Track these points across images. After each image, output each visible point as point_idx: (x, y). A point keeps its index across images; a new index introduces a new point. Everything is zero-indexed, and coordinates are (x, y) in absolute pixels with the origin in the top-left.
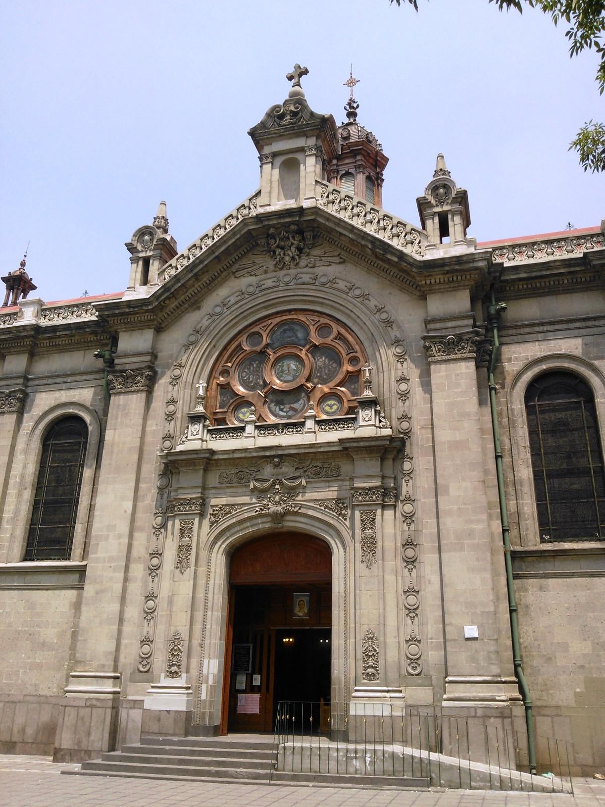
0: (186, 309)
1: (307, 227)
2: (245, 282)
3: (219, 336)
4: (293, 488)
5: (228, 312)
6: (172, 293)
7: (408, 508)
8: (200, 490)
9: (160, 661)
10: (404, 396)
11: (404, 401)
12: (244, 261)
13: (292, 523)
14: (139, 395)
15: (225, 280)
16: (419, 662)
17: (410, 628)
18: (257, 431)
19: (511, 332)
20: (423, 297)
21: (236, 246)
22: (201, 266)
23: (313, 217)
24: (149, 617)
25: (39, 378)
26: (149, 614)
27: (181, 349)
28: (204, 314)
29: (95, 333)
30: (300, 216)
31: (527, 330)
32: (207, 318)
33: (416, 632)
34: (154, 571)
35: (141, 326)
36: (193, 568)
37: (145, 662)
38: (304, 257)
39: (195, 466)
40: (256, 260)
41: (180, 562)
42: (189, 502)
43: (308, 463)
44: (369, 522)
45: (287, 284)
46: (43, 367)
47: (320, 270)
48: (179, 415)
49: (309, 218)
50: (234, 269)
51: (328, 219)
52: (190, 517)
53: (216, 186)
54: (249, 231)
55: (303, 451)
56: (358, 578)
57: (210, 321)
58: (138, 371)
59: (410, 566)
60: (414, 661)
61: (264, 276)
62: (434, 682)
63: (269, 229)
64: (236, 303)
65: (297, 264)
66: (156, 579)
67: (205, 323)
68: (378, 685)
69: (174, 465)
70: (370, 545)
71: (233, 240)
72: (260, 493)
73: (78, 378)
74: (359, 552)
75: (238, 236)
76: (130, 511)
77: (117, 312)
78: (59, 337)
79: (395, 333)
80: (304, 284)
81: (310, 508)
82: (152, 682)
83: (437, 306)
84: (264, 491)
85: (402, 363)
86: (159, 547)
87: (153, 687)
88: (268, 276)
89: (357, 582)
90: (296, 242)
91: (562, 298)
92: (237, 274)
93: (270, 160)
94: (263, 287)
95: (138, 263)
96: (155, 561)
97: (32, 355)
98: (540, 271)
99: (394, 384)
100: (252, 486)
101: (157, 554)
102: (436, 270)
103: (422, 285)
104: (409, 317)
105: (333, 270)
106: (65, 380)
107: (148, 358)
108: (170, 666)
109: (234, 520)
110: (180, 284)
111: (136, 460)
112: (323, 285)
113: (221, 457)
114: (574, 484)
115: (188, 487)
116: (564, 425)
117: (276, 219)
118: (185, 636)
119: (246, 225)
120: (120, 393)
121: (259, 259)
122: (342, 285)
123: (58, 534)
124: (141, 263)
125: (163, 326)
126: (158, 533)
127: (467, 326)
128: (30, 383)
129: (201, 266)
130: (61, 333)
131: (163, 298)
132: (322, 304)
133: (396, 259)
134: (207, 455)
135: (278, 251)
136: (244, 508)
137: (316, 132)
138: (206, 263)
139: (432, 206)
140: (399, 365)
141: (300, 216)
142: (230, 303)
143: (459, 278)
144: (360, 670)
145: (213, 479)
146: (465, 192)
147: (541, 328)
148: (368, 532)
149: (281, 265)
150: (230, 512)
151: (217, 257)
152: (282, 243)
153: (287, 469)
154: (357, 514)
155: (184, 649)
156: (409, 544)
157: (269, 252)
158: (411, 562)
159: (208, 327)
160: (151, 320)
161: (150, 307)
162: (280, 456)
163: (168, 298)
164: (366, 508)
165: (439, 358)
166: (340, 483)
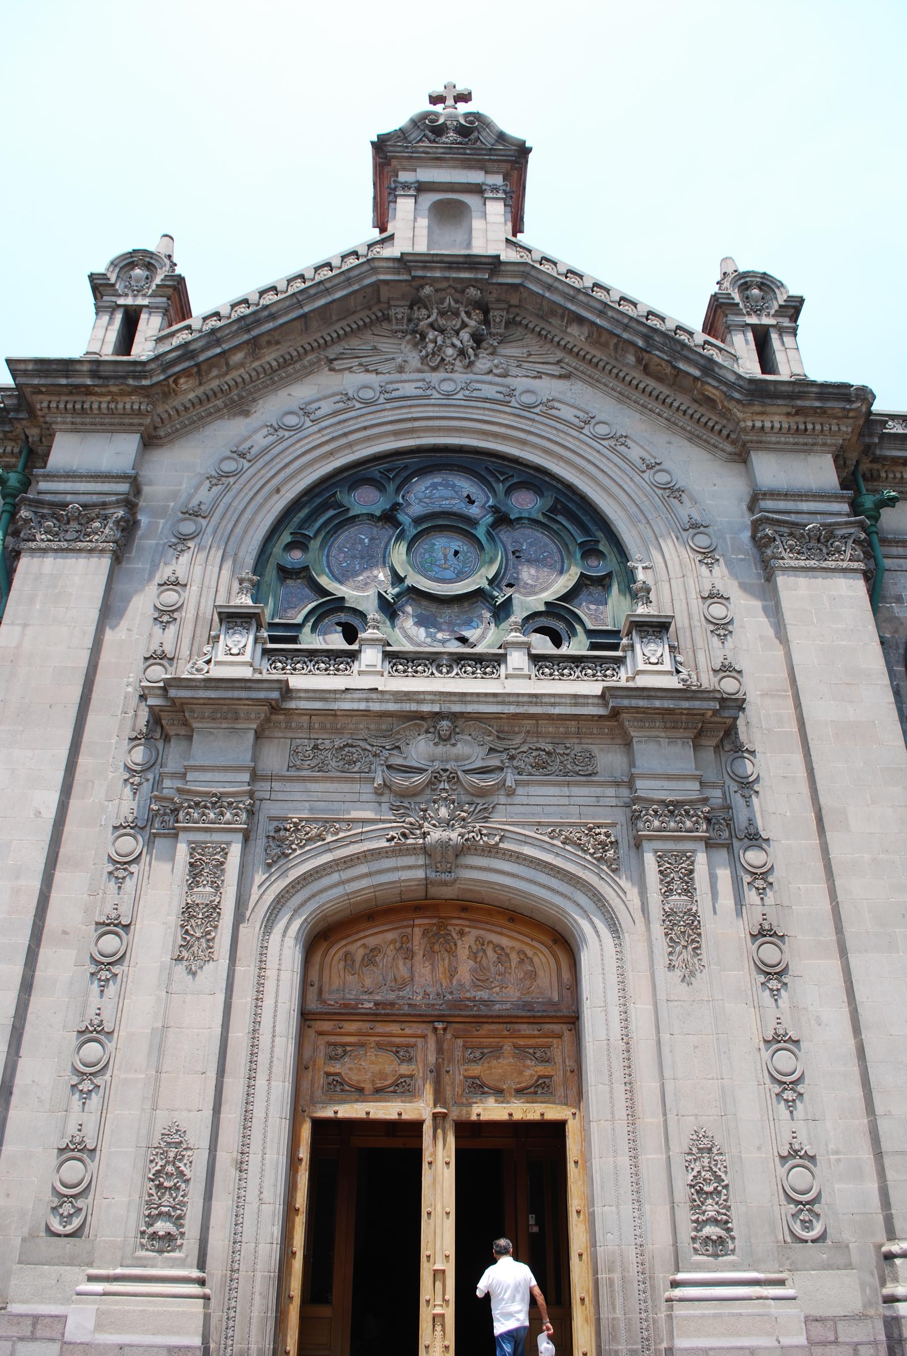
0: (219, 410)
1: (498, 301)
2: (353, 381)
3: (288, 471)
4: (483, 793)
5: (315, 428)
6: (198, 365)
7: (753, 857)
8: (246, 777)
9: (117, 1203)
10: (722, 628)
11: (723, 638)
12: (354, 342)
15: (308, 371)
16: (816, 1208)
17: (788, 1128)
18: (387, 666)
19: (894, 551)
20: (741, 457)
21: (342, 309)
22: (271, 325)
23: (517, 281)
24: (86, 1086)
26: (87, 1079)
27: (201, 483)
32: (265, 431)
33: (802, 1137)
34: (106, 968)
35: (112, 424)
36: (224, 962)
37: (67, 1209)
38: (483, 354)
41: (186, 946)
42: (218, 801)
43: (518, 740)
45: (448, 395)
47: (520, 383)
48: (189, 614)
50: (331, 353)
51: (550, 287)
52: (217, 837)
53: (277, 219)
54: (377, 285)
56: (662, 1005)
57: (271, 438)
59: (774, 984)
60: (806, 1206)
61: (397, 376)
62: (855, 1258)
63: (422, 287)
65: (471, 364)
66: (112, 989)
67: (260, 440)
68: (734, 1267)
70: (684, 930)
74: (661, 944)
75: (356, 287)
76: (50, 813)
77: (63, 381)
79: (685, 511)
80: (486, 400)
82: (90, 1264)
83: (771, 470)
84: (406, 794)
85: (709, 566)
86: (123, 910)
87: (91, 1279)
88: (404, 376)
89: (663, 1013)
90: (472, 323)
92: (337, 365)
94: (395, 394)
96: (110, 943)
99: (696, 604)
100: (379, 781)
101: (116, 926)
102: (780, 402)
103: (744, 430)
104: (717, 489)
105: (548, 388)
107: (124, 487)
108: (151, 1220)
110: (218, 350)
111: (77, 699)
112: (528, 407)
113: (303, 705)
115: (217, 761)
117: (441, 269)
118: (198, 1138)
119: (375, 270)
120: (45, 551)
121: (386, 345)
122: (567, 413)
124: (119, 317)
125: (162, 433)
126: (121, 874)
127: (839, 514)
129: (271, 325)
131: (177, 369)
132: (524, 443)
134: (275, 695)
135: (431, 335)
136: (359, 834)
138: (281, 321)
139: (739, 313)
140: (704, 570)
142: (319, 413)
143: (818, 427)
144: (686, 1231)
145: (275, 758)
146: (801, 300)
148: (678, 900)
151: (304, 316)
152: (442, 322)
153: (469, 751)
154: (650, 859)
155: (196, 1171)
156: (765, 934)
157: (414, 332)
158: (774, 975)
159: (265, 450)
160: (139, 413)
161: (145, 382)
162: (454, 717)
163: (186, 372)
164: (670, 845)
165: (793, 563)
166: (598, 791)
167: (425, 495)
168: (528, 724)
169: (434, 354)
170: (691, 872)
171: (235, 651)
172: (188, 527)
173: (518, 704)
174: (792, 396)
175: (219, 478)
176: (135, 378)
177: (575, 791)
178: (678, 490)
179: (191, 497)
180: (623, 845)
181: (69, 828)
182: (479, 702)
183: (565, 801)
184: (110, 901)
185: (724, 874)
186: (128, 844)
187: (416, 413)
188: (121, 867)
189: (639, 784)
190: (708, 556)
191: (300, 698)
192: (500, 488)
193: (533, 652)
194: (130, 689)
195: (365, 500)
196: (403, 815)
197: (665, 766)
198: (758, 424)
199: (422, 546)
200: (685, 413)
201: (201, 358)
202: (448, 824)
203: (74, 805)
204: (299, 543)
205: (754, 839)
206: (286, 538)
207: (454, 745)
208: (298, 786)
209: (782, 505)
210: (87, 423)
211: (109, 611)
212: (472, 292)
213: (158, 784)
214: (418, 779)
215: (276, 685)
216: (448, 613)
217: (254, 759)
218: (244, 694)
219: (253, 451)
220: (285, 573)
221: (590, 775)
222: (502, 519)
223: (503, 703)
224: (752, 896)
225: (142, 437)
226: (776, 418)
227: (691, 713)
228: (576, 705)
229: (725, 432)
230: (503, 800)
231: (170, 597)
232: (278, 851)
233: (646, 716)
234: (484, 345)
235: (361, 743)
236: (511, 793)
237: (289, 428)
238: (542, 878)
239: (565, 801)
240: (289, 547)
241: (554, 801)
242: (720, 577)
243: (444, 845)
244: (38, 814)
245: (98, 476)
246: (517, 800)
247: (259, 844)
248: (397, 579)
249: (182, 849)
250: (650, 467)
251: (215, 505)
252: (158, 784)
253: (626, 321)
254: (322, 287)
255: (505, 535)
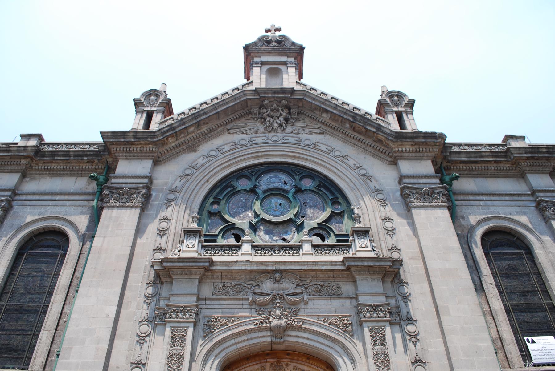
0: (184, 150)
1: (294, 105)
2: (237, 137)
3: (212, 173)
4: (294, 304)
5: (223, 156)
6: (176, 132)
7: (410, 328)
8: (195, 299)
10: (391, 232)
11: (391, 236)
12: (238, 122)
13: (295, 338)
14: (133, 210)
15: (219, 134)
18: (253, 251)
19: (459, 198)
21: (233, 110)
22: (205, 117)
23: (301, 97)
25: (27, 194)
27: (177, 179)
28: (200, 155)
29: (90, 162)
30: (291, 95)
31: (471, 198)
32: (202, 158)
35: (141, 156)
38: (289, 125)
39: (191, 274)
40: (248, 124)
42: (183, 310)
43: (308, 281)
44: (379, 339)
45: (275, 142)
46: (31, 186)
47: (304, 136)
48: (171, 231)
49: (299, 97)
50: (229, 127)
51: (314, 99)
52: (182, 325)
55: (306, 268)
57: (205, 161)
58: (132, 191)
61: (255, 135)
63: (264, 100)
64: (230, 150)
65: (284, 129)
67: (201, 161)
69: (165, 273)
71: (234, 103)
72: (261, 307)
73: (67, 198)
75: (238, 101)
78: (56, 162)
79: (373, 184)
80: (290, 143)
81: (313, 324)
83: (407, 167)
84: (262, 305)
86: (142, 357)
90: (284, 114)
91: (488, 179)
92: (231, 131)
93: (259, 65)
94: (254, 142)
95: (142, 113)
97: (24, 176)
98: (476, 157)
99: (379, 222)
100: (251, 299)
102: (408, 140)
104: (385, 176)
105: (315, 138)
106: (54, 198)
107: (146, 181)
109: (229, 333)
110: (184, 127)
112: (308, 146)
114: (534, 317)
115: (183, 292)
116: (514, 270)
117: (272, 94)
121: (250, 123)
122: (323, 147)
123: (17, 341)
124: (145, 115)
126: (142, 341)
128: (17, 198)
129: (205, 117)
130: (59, 158)
131: (168, 134)
132: (306, 160)
133: (374, 130)
135: (268, 119)
137: (295, 55)
139: (390, 107)
140: (382, 208)
141: (291, 95)
142: (224, 150)
145: (207, 291)
146: (414, 101)
147: (481, 198)
148: (379, 348)
149: (270, 129)
150: (226, 324)
151: (218, 113)
152: (272, 114)
153: (288, 286)
154: (366, 330)
159: (203, 165)
161: (155, 140)
162: (281, 272)
163: (171, 136)
164: (374, 324)
165: (418, 204)
167: (267, 181)
168: (313, 274)
169: (269, 126)
170: (384, 335)
171: (190, 246)
172: (171, 196)
173: (308, 265)
174: (413, 138)
175: (184, 176)
176: (151, 138)
177: (334, 302)
178: (370, 176)
179: (173, 184)
180: (355, 324)
181: (121, 322)
182: (291, 265)
183: (329, 306)
184: (137, 353)
185: (398, 336)
186: (145, 328)
187: (263, 149)
188: (142, 338)
189: (360, 298)
190: (383, 202)
191: (217, 265)
192: (297, 178)
193: (313, 244)
194: (147, 263)
195: (243, 184)
196: (261, 314)
197: (371, 290)
198: (400, 149)
199: (266, 202)
200: (370, 146)
201: (177, 130)
202: (280, 317)
203: (123, 311)
204: (217, 202)
205: (410, 320)
206: (211, 200)
207: (282, 283)
208: (217, 302)
209: (412, 181)
210: (132, 156)
211: (139, 231)
212: (284, 102)
213: (158, 302)
214: (267, 298)
215: (207, 260)
216: (278, 229)
217: (198, 291)
218: (194, 264)
219: (198, 166)
220: (211, 214)
221: (339, 295)
222: (299, 190)
223: (302, 265)
224: (411, 345)
225: (153, 161)
226: (407, 147)
227: (380, 267)
228: (332, 265)
229: (387, 153)
230: (303, 306)
231: (164, 225)
232: (208, 330)
233: (361, 269)
234: (289, 122)
235: (243, 284)
236: (306, 303)
237: (212, 156)
238: (321, 340)
239: (329, 306)
240: (212, 203)
241: (324, 306)
242: (389, 211)
243: (279, 326)
244: (108, 316)
245: (136, 177)
246: (309, 306)
247: (201, 327)
248: (257, 215)
249: (168, 330)
250: (357, 168)
251: (182, 187)
252: (158, 302)
253: (345, 111)
254: (225, 102)
255: (300, 196)
